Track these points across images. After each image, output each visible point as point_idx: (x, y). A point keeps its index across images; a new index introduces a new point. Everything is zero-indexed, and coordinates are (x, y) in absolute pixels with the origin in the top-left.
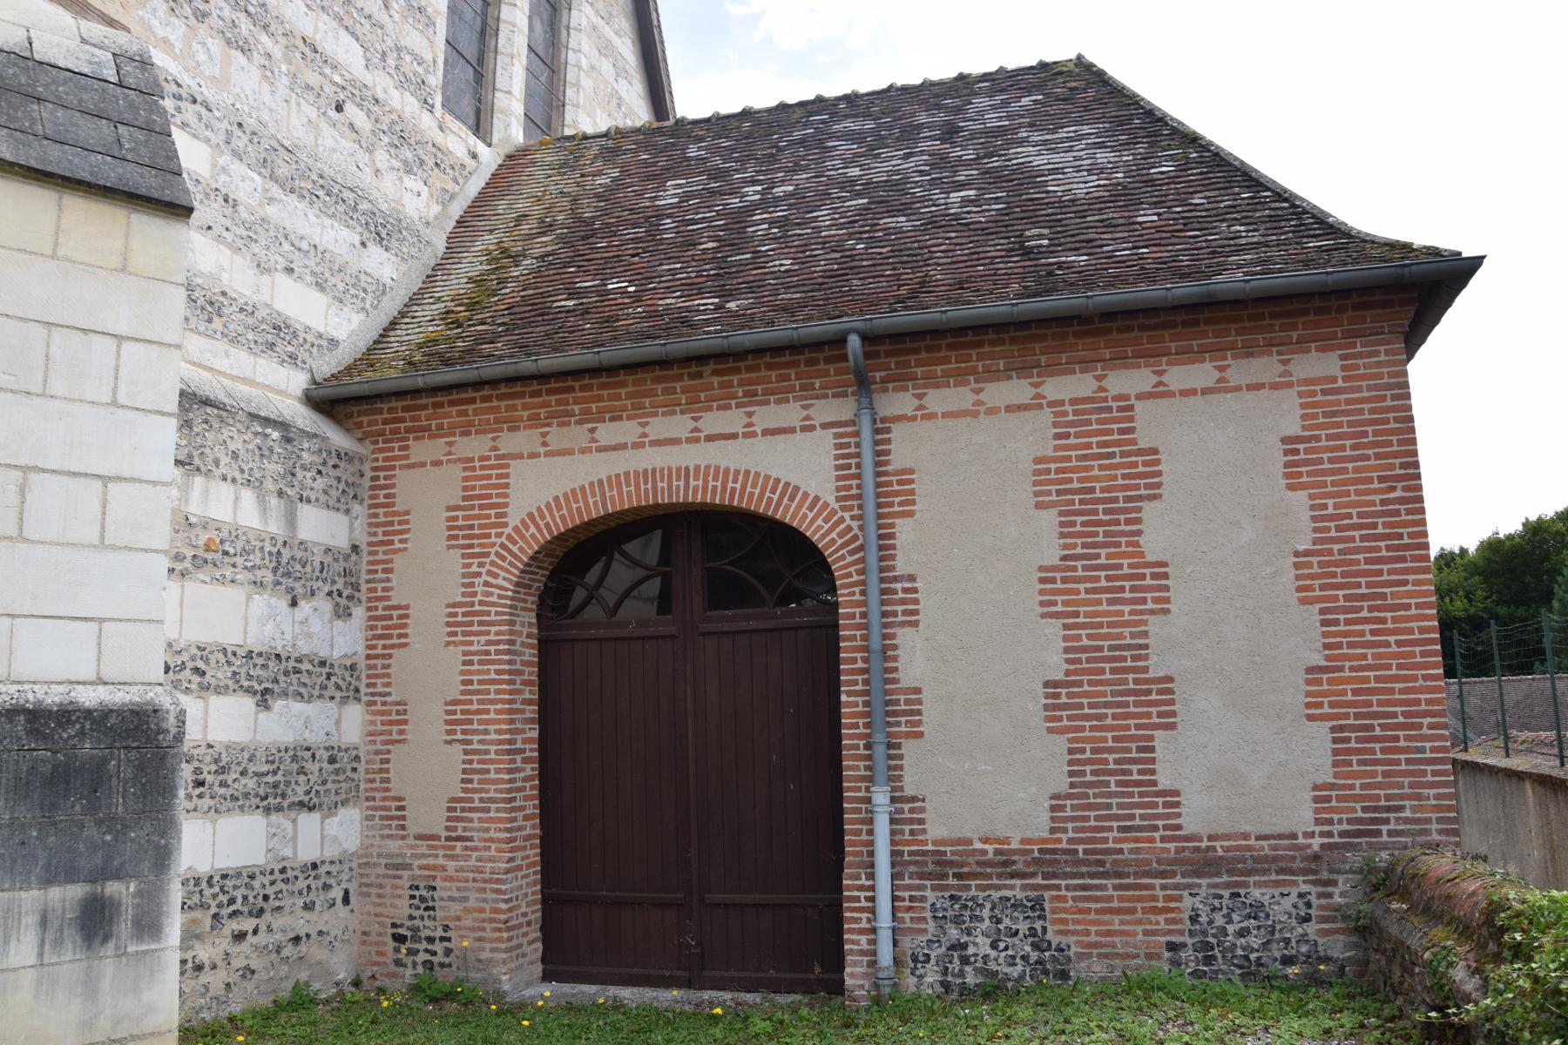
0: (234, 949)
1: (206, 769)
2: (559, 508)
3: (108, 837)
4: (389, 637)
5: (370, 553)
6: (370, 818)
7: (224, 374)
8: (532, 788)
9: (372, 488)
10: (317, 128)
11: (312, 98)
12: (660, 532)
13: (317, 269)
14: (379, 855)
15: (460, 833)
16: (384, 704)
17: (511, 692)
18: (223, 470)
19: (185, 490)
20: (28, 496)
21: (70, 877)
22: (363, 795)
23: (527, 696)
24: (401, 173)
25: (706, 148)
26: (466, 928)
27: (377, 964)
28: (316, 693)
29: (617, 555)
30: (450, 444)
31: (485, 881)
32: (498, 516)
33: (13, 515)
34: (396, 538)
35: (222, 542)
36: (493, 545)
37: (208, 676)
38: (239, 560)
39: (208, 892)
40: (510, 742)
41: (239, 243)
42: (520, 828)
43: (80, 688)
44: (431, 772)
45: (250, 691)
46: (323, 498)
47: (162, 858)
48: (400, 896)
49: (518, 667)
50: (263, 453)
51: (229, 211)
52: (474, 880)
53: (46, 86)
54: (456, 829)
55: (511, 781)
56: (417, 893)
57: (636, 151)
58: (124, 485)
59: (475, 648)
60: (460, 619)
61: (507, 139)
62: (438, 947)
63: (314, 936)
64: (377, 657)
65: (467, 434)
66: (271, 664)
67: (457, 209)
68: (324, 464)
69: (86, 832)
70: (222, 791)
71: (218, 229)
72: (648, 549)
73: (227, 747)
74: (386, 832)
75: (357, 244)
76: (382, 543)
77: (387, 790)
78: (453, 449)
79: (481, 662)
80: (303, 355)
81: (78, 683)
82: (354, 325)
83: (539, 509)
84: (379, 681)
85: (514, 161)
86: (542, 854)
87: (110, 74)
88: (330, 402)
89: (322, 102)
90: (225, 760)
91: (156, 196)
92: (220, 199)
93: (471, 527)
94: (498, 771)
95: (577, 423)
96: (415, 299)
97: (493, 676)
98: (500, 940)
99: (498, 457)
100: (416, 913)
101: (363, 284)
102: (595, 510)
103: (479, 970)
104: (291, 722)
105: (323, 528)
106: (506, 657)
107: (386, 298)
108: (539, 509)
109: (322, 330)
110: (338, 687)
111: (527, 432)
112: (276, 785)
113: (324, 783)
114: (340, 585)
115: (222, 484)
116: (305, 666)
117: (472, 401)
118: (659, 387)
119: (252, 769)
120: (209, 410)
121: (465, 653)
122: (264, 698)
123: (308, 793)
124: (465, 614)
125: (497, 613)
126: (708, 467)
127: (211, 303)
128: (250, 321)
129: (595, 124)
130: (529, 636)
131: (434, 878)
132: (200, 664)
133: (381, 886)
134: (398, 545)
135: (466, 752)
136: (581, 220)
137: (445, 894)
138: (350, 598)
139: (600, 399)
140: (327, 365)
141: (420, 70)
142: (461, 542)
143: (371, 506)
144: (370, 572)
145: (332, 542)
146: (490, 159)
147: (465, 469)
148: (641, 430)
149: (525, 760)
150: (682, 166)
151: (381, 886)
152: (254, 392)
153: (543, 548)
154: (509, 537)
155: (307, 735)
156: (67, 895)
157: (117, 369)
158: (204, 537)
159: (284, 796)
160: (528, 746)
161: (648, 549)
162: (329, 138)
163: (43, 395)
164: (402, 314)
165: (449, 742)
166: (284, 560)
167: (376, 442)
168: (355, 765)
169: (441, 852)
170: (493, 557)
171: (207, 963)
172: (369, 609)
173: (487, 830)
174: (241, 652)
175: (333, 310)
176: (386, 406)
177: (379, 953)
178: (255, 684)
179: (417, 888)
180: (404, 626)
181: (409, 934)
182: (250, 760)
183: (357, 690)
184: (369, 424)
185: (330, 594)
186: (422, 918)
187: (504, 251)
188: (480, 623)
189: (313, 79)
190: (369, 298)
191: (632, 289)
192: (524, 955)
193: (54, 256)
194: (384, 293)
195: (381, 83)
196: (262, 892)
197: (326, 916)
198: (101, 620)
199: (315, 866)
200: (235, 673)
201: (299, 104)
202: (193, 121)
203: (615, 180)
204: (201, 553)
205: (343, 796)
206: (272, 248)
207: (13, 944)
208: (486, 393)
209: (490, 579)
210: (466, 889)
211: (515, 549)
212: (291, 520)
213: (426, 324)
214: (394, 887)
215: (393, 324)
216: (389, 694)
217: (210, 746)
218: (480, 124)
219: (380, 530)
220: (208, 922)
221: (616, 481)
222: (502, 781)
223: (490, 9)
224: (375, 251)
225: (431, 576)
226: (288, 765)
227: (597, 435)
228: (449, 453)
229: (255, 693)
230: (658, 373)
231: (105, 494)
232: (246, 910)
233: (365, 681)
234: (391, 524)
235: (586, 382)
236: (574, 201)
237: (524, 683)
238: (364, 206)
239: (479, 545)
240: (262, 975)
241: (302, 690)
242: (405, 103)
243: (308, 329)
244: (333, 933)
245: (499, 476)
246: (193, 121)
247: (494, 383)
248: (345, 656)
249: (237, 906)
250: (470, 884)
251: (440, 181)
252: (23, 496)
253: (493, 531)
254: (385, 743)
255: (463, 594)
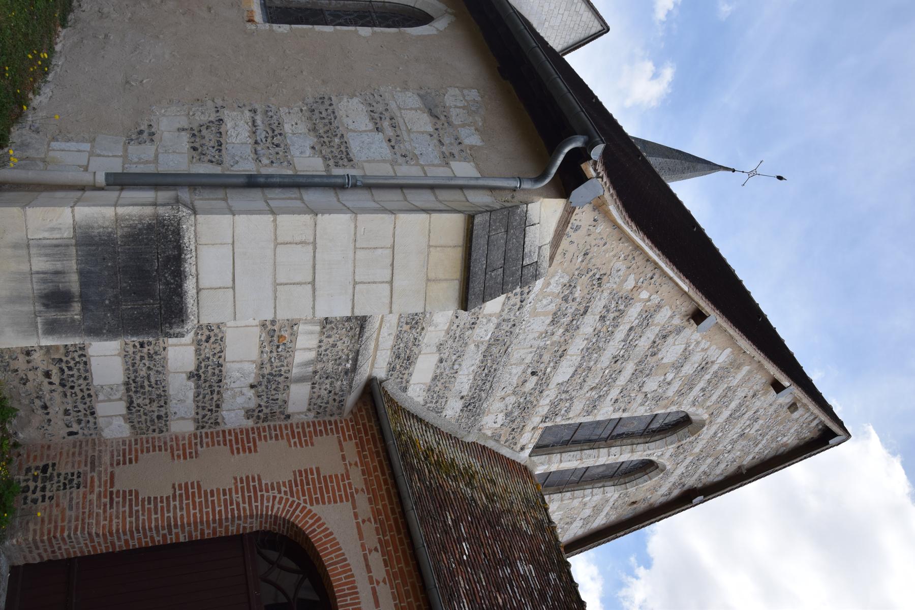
0: (39, 372)
1: (150, 348)
2: (326, 536)
3: (107, 302)
4: (237, 443)
5: (286, 426)
6: (124, 443)
7: (379, 334)
8: (146, 542)
9: (324, 422)
10: (521, 364)
11: (535, 359)
12: (317, 599)
13: (444, 375)
14: (100, 451)
15: (116, 500)
16: (196, 444)
17: (208, 521)
18: (325, 340)
19: (312, 322)
20: (300, 246)
21: (83, 284)
22: (139, 437)
23: (206, 532)
24: (505, 411)
25: (556, 584)
26: (51, 511)
27: (28, 456)
28: (200, 404)
29: (301, 576)
30: (356, 464)
31: (83, 520)
32: (317, 499)
33: (289, 239)
34: (296, 440)
35: (284, 344)
36: (299, 499)
37: (207, 344)
38: (275, 354)
39: (76, 355)
40: (176, 526)
41: (452, 333)
42: (119, 538)
43: (194, 280)
44: (154, 477)
45: (198, 367)
46: (315, 396)
47: (96, 332)
48: (73, 466)
49: (224, 524)
50: (338, 360)
51: (468, 326)
52: (84, 513)
53: (514, 233)
54: (118, 497)
55: (150, 529)
56: (75, 477)
57: (545, 541)
58: (311, 292)
59: (234, 495)
60: (251, 484)
61: (535, 465)
62: (38, 494)
63: (48, 417)
64: (224, 437)
65: (363, 474)
66: (215, 378)
67: (491, 444)
68: (335, 394)
69: (110, 291)
70: (138, 358)
71: (457, 321)
72: (308, 594)
73: (164, 358)
74: (115, 454)
75: (462, 394)
76: (293, 432)
77: (142, 451)
78: (353, 466)
79: (225, 500)
80: (396, 374)
81: (197, 279)
82: (416, 399)
83: (323, 524)
84: (209, 440)
85: (524, 471)
86: (102, 554)
87: (527, 261)
88: (372, 392)
89: (535, 364)
90: (157, 357)
91: (471, 292)
92: (473, 320)
93: (308, 484)
94: (157, 519)
95: (379, 539)
96: (436, 430)
97: (217, 509)
98: (42, 534)
99: (352, 494)
100: (62, 478)
101: (440, 400)
102: (327, 559)
103: (21, 523)
104: (181, 391)
105: (298, 397)
106: (230, 516)
107: (434, 414)
108: (323, 524)
109: (411, 382)
110: (204, 416)
111: (369, 510)
112: (142, 387)
113: (145, 414)
114: (265, 411)
115: (317, 341)
116: (215, 397)
117: (383, 474)
118: (409, 588)
119: (152, 373)
120: (358, 329)
121: (230, 490)
122: (194, 376)
123: (139, 405)
124: (254, 487)
125: (257, 507)
126: (357, 593)
127: (417, 323)
128: (410, 344)
129: (554, 512)
130: (244, 528)
131: (85, 487)
132: (212, 339)
133: (80, 454)
134: (292, 441)
135: (168, 498)
136: (499, 517)
137: (74, 495)
138: (258, 418)
139: (396, 551)
140: (391, 387)
141: (563, 412)
142: (298, 479)
143: (314, 423)
144: (275, 427)
145: (290, 403)
146: (523, 457)
147: (342, 475)
148: (381, 580)
149: (164, 536)
150: (542, 571)
151: (80, 454)
152: (371, 351)
153: (300, 529)
154: (304, 508)
155: (174, 401)
156: (73, 283)
157: (375, 283)
158: (286, 334)
159: (136, 392)
160: (174, 536)
161: (308, 594)
162: (517, 370)
163: (355, 248)
164: (427, 424)
165: (174, 487)
166: (277, 379)
167: (351, 421)
168: (157, 431)
169: (102, 489)
170: (291, 499)
171: (31, 358)
172: (253, 429)
173: (117, 517)
174: (221, 361)
175: (423, 387)
176: (373, 424)
177: (35, 457)
178: (203, 370)
179: (79, 477)
180: (244, 451)
181: (48, 475)
182: (157, 371)
183: (203, 427)
184: (361, 416)
185: (260, 406)
186: (59, 482)
187: (472, 477)
188: (250, 497)
189: (546, 357)
190: (433, 405)
191: (465, 557)
192: (31, 552)
193: (429, 246)
194: (437, 412)
195: (551, 393)
196: (76, 385)
197: (61, 423)
198: (233, 288)
199: (93, 413)
200: (208, 358)
201: (531, 352)
202: (512, 302)
203: (526, 532)
204: (277, 333)
205: (137, 426)
206: (451, 351)
207: (45, 259)
208: (389, 481)
209: (277, 499)
210: (78, 508)
211: (297, 512)
212: (301, 380)
213: (424, 439)
214: (80, 462)
215: (420, 420)
216: (202, 447)
217: (164, 349)
218: (541, 448)
219: (300, 430)
220: (57, 356)
221: (347, 569)
222: (150, 523)
223: (603, 442)
224: (459, 404)
225: (276, 463)
226: (155, 393)
227: (374, 552)
228: (350, 465)
229: (197, 370)
230: (417, 585)
231: (305, 283)
232: (65, 376)
233: (209, 431)
234: (305, 436)
235: (405, 541)
236: (509, 511)
237: (215, 529)
238: (483, 395)
239: (298, 490)
240: (22, 389)
241: (201, 396)
242: (543, 406)
243: (410, 375)
244: (49, 428)
245: (340, 496)
246: (512, 302)
247: (396, 484)
248: (223, 418)
249: (67, 372)
250: (81, 510)
251: (505, 433)
252: (300, 243)
253: (307, 497)
254: (172, 447)
255: (266, 484)
